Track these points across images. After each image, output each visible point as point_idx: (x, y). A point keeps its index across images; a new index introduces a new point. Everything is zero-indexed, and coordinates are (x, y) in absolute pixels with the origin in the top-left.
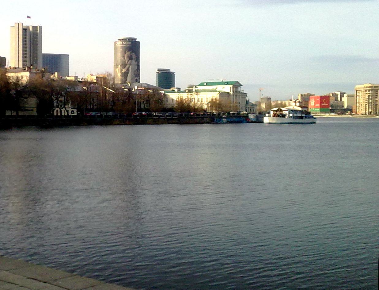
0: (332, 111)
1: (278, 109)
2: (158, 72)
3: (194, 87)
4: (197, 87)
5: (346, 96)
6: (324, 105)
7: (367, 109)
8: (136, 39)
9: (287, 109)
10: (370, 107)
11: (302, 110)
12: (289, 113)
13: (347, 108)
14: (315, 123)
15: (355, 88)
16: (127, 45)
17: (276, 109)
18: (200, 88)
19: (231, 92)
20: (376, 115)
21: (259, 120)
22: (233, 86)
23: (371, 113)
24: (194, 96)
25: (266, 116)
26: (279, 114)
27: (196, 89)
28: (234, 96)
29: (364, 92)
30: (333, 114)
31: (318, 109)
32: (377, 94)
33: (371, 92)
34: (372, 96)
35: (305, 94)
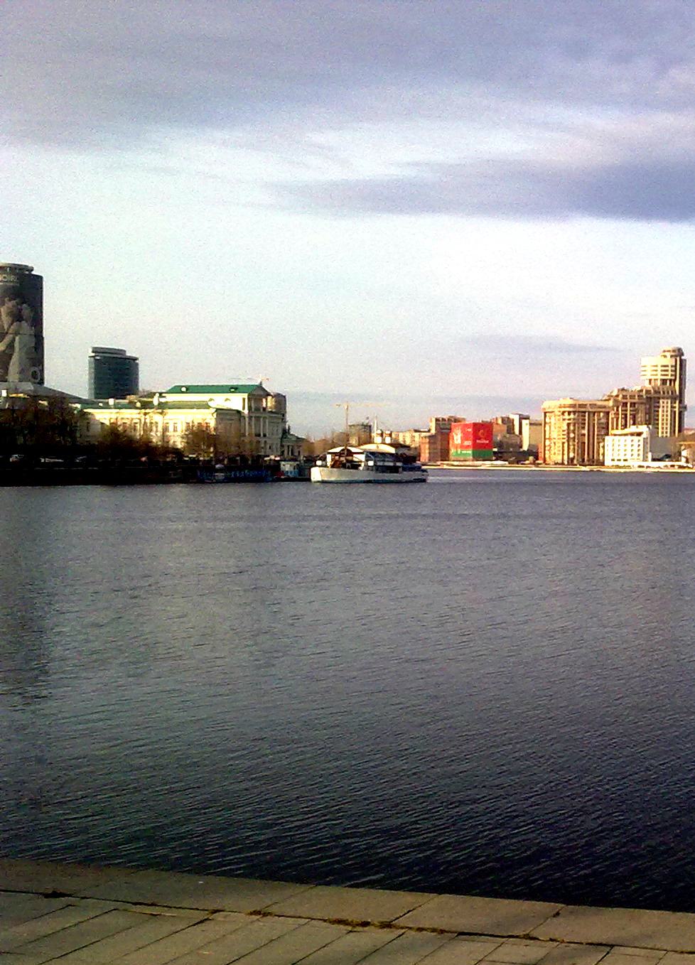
0: (498, 456)
1: (343, 450)
2: (93, 354)
3: (158, 395)
4: (164, 397)
5: (527, 424)
6: (482, 442)
7: (566, 452)
8: (32, 270)
9: (362, 451)
10: (572, 447)
11: (397, 454)
12: (367, 461)
13: (528, 450)
14: (424, 481)
15: (542, 407)
16: (8, 284)
17: (338, 450)
18: (171, 398)
19: (244, 409)
20: (583, 465)
21: (302, 476)
22: (248, 396)
23: (572, 459)
24: (155, 417)
25: (316, 466)
26: (345, 461)
27: (162, 400)
28: (253, 419)
29: (559, 416)
30: (499, 462)
31: (470, 452)
32: (585, 420)
33: (572, 416)
34: (574, 426)
35: (445, 417)
